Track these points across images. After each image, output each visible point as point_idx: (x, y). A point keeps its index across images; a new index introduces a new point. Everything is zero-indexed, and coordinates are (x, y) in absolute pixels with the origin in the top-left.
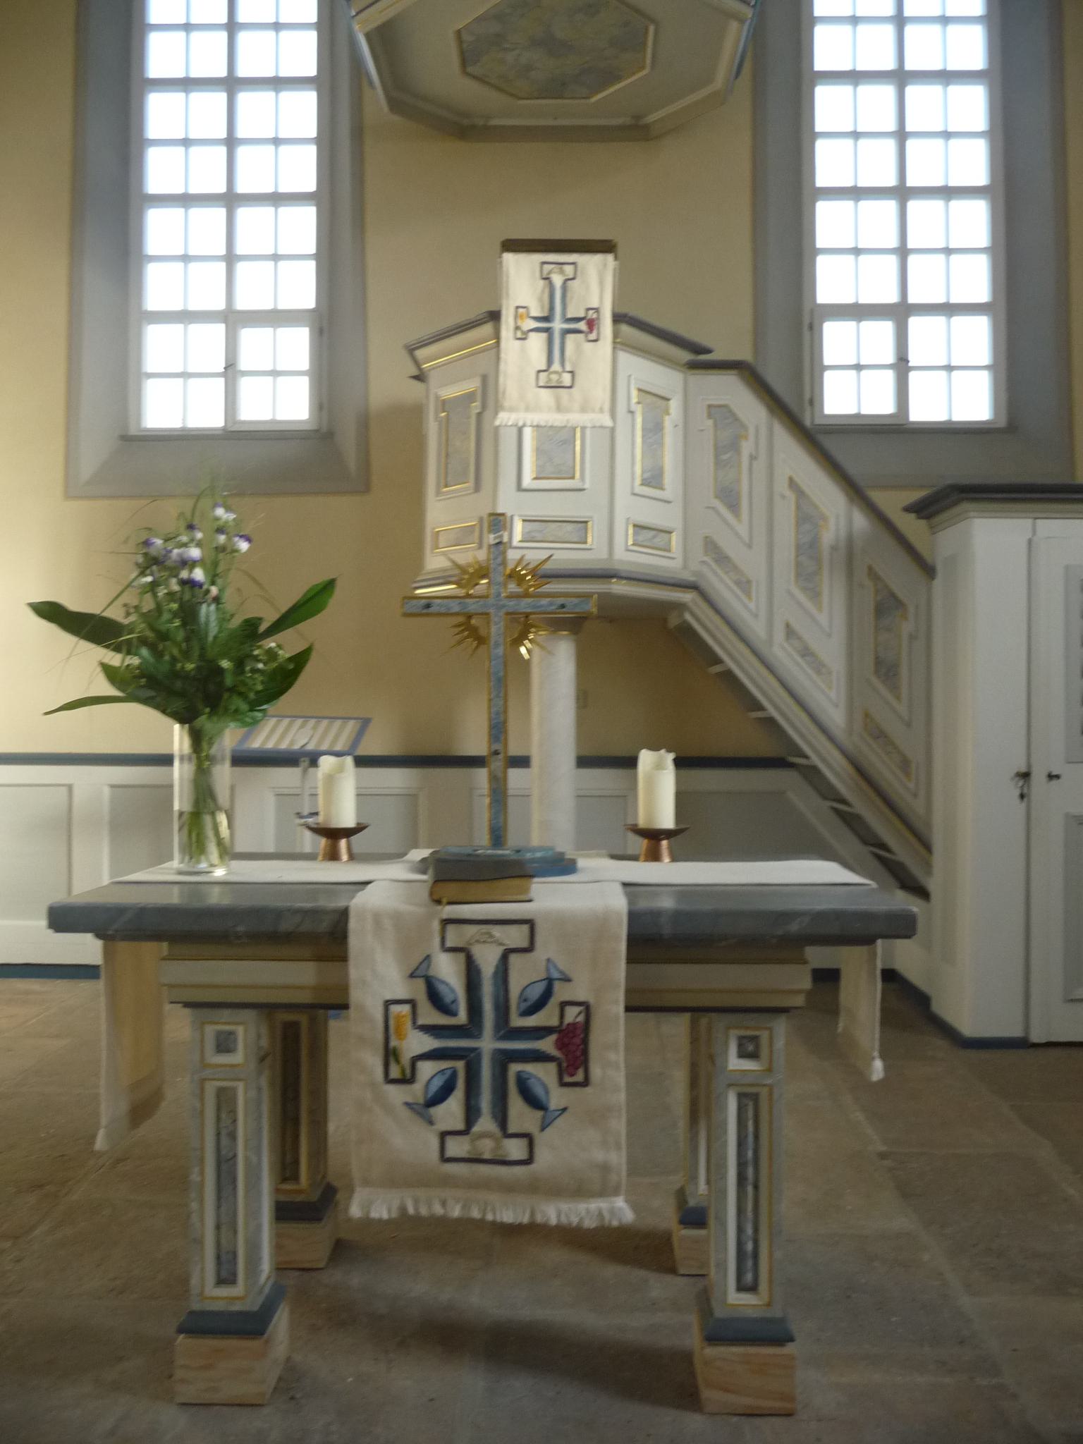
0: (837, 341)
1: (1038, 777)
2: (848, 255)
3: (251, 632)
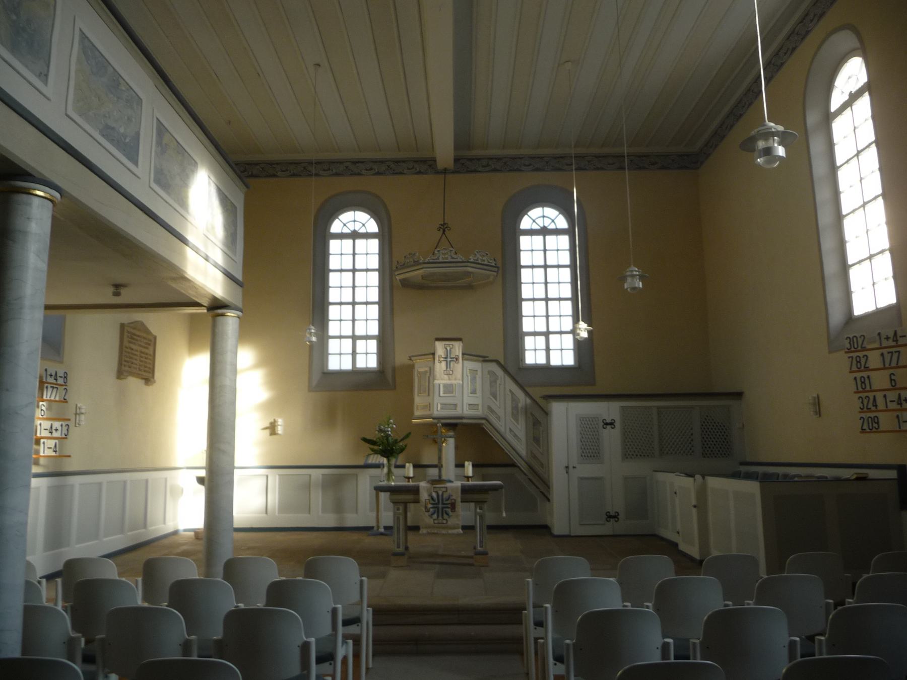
0: (529, 342)
1: (571, 467)
2: (532, 317)
3: (396, 442)
